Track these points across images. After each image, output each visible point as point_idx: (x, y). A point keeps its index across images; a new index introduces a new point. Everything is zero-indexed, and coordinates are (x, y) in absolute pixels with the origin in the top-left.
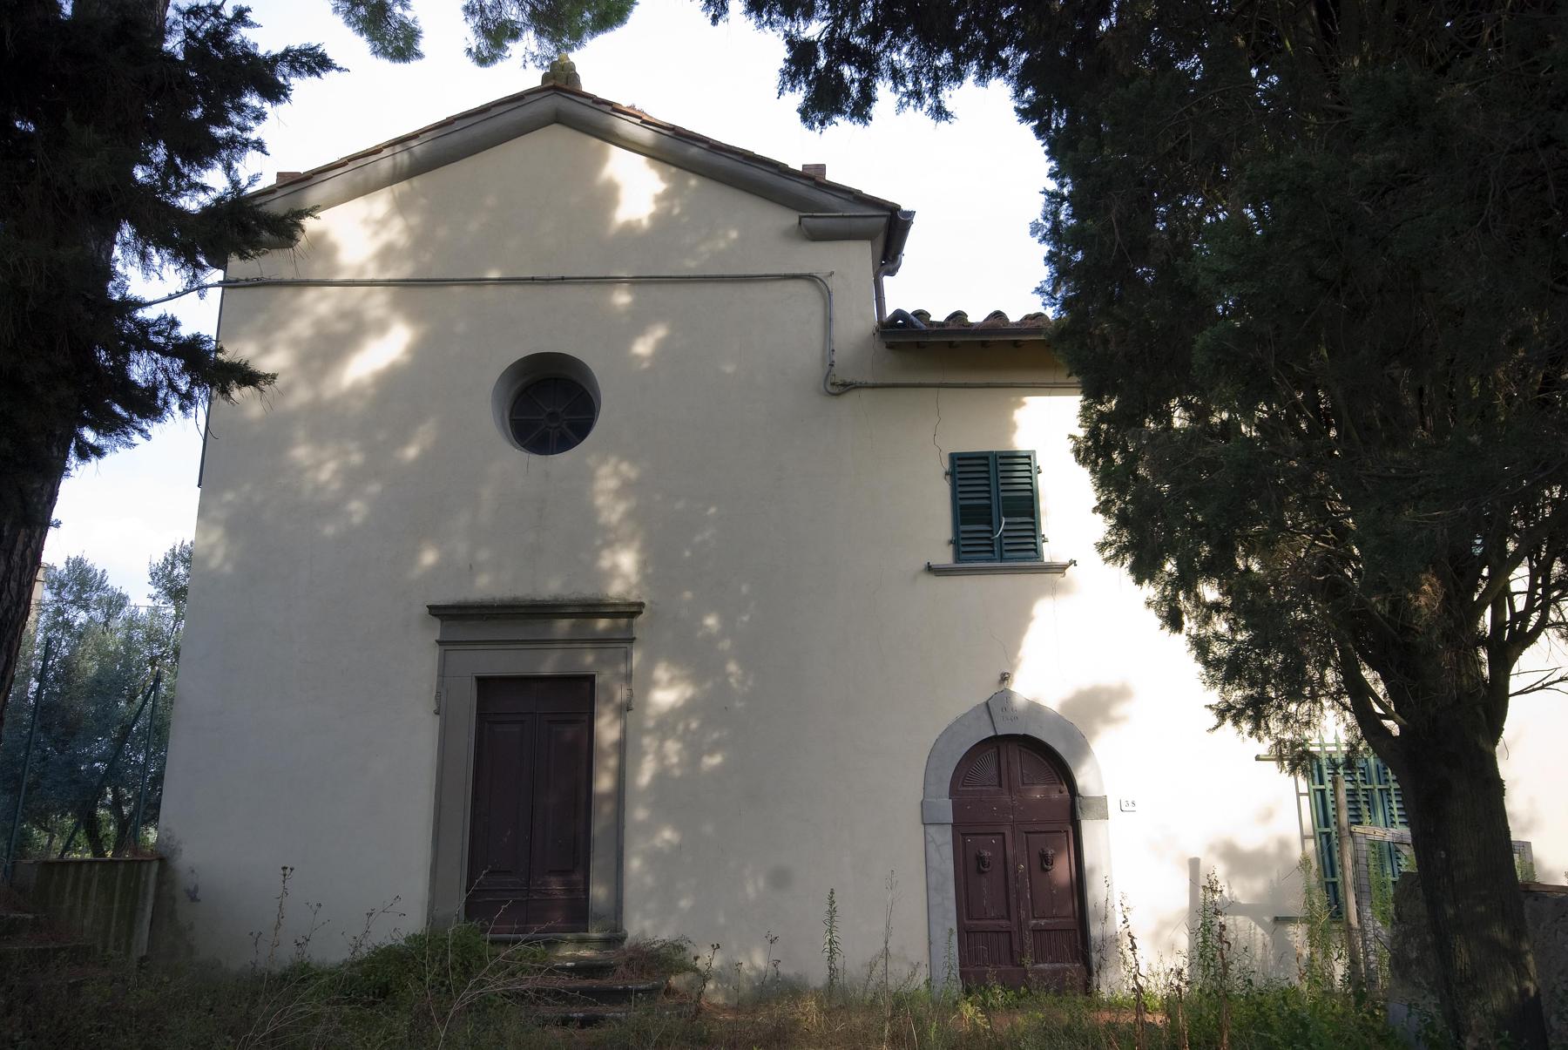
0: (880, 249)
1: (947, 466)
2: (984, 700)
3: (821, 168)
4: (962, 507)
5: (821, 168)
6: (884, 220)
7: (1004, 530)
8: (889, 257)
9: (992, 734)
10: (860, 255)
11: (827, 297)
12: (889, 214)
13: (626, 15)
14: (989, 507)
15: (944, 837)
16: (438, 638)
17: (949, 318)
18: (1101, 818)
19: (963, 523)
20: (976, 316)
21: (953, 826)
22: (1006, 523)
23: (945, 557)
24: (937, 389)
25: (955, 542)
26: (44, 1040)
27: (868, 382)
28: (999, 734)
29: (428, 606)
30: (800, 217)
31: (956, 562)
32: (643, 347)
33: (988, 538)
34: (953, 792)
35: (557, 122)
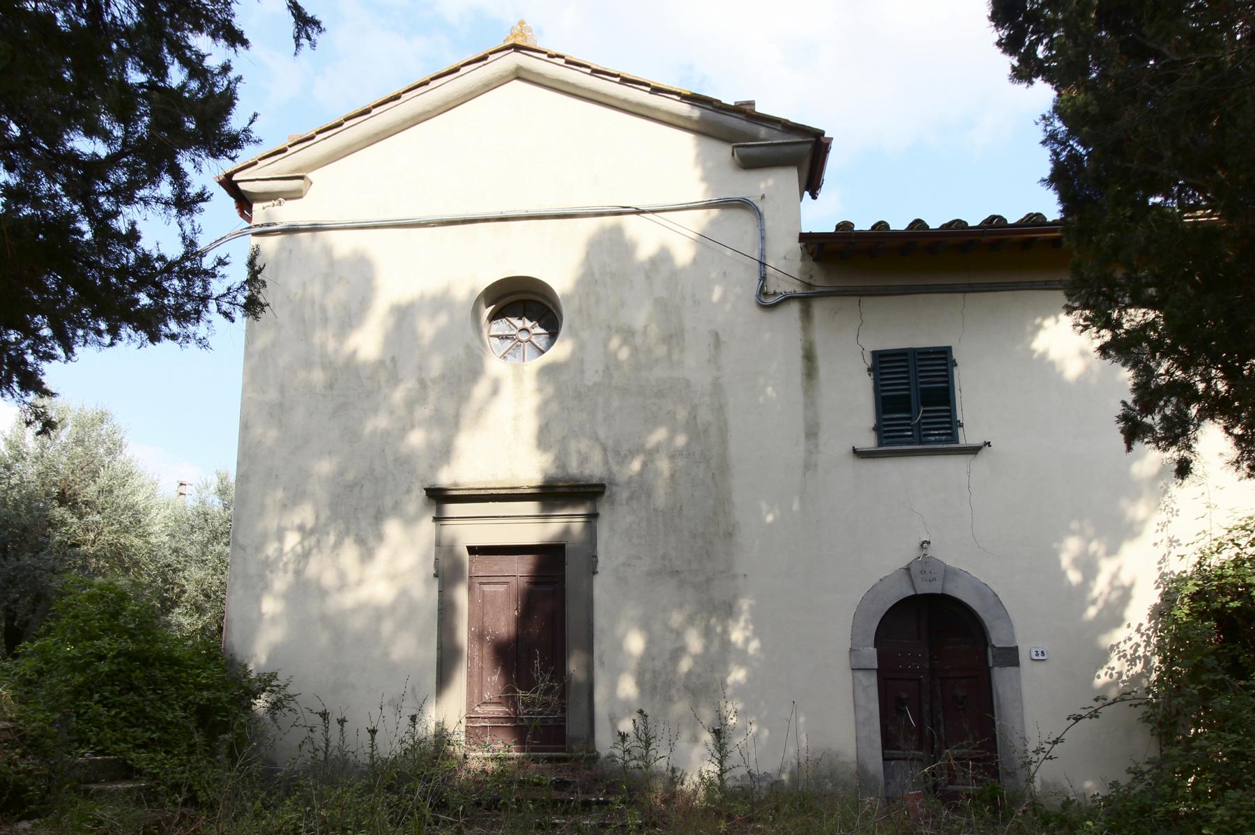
0: (805, 176)
1: (869, 362)
2: (904, 565)
3: (752, 103)
4: (884, 398)
5: (752, 103)
6: (809, 146)
7: (923, 418)
8: (812, 184)
9: (912, 593)
10: (788, 179)
11: (760, 216)
12: (814, 139)
13: (794, 779)
14: (908, 397)
15: (871, 681)
16: (434, 515)
17: (873, 227)
18: (1012, 665)
19: (884, 412)
20: (899, 223)
21: (879, 671)
22: (924, 412)
23: (868, 441)
24: (962, 294)
25: (877, 429)
26: (243, 721)
27: (788, 291)
28: (919, 593)
29: (425, 489)
30: (734, 147)
31: (879, 446)
32: (143, 6)
33: (908, 425)
34: (878, 643)
35: (518, 78)
